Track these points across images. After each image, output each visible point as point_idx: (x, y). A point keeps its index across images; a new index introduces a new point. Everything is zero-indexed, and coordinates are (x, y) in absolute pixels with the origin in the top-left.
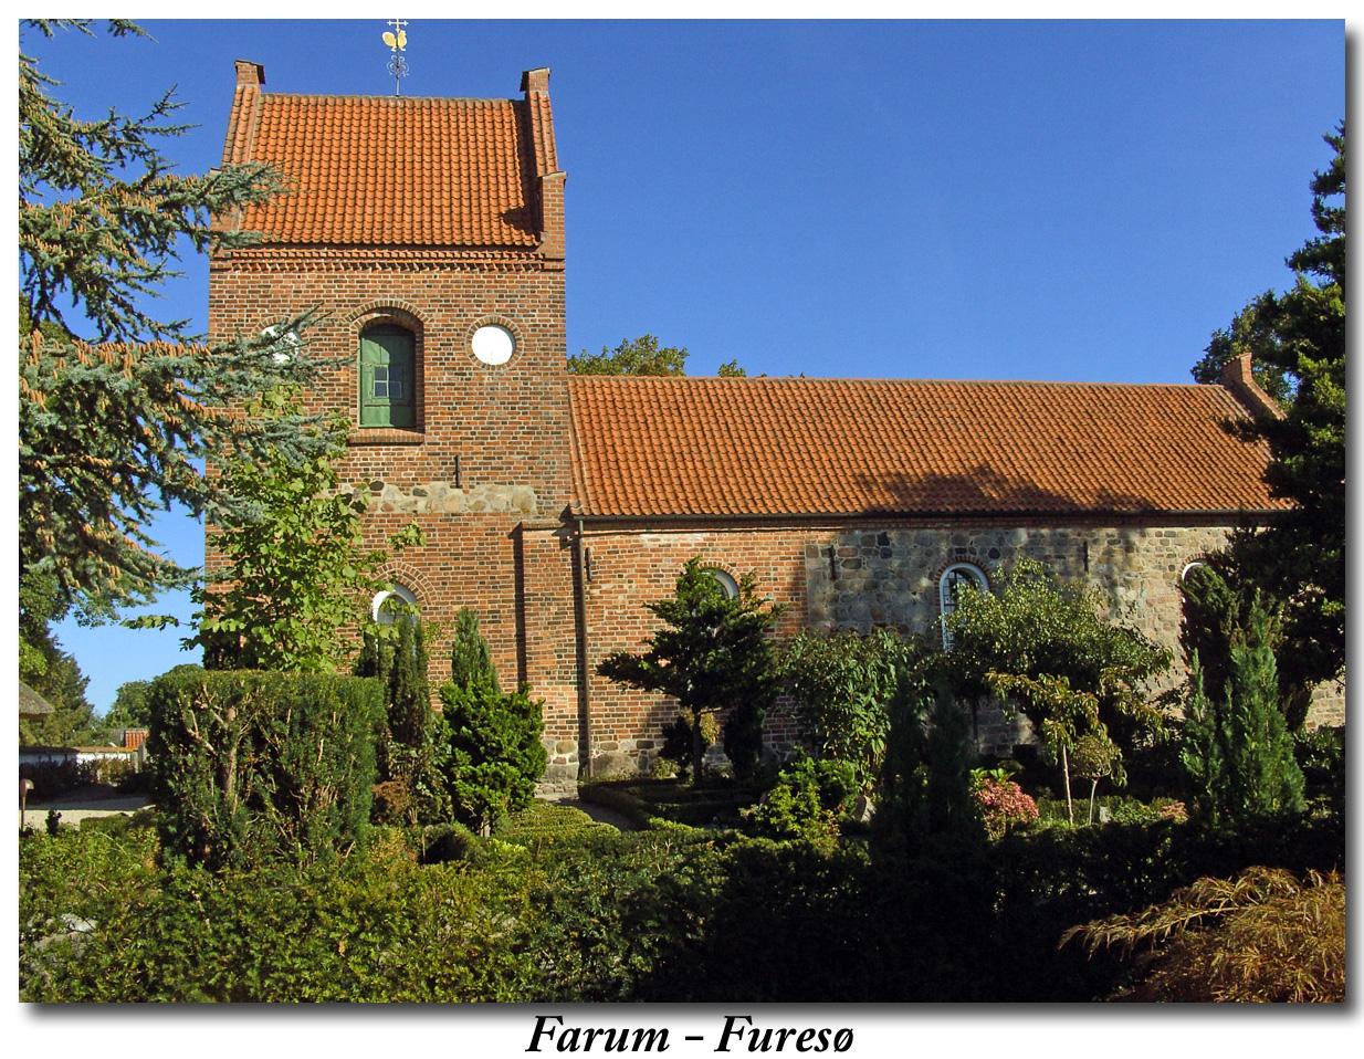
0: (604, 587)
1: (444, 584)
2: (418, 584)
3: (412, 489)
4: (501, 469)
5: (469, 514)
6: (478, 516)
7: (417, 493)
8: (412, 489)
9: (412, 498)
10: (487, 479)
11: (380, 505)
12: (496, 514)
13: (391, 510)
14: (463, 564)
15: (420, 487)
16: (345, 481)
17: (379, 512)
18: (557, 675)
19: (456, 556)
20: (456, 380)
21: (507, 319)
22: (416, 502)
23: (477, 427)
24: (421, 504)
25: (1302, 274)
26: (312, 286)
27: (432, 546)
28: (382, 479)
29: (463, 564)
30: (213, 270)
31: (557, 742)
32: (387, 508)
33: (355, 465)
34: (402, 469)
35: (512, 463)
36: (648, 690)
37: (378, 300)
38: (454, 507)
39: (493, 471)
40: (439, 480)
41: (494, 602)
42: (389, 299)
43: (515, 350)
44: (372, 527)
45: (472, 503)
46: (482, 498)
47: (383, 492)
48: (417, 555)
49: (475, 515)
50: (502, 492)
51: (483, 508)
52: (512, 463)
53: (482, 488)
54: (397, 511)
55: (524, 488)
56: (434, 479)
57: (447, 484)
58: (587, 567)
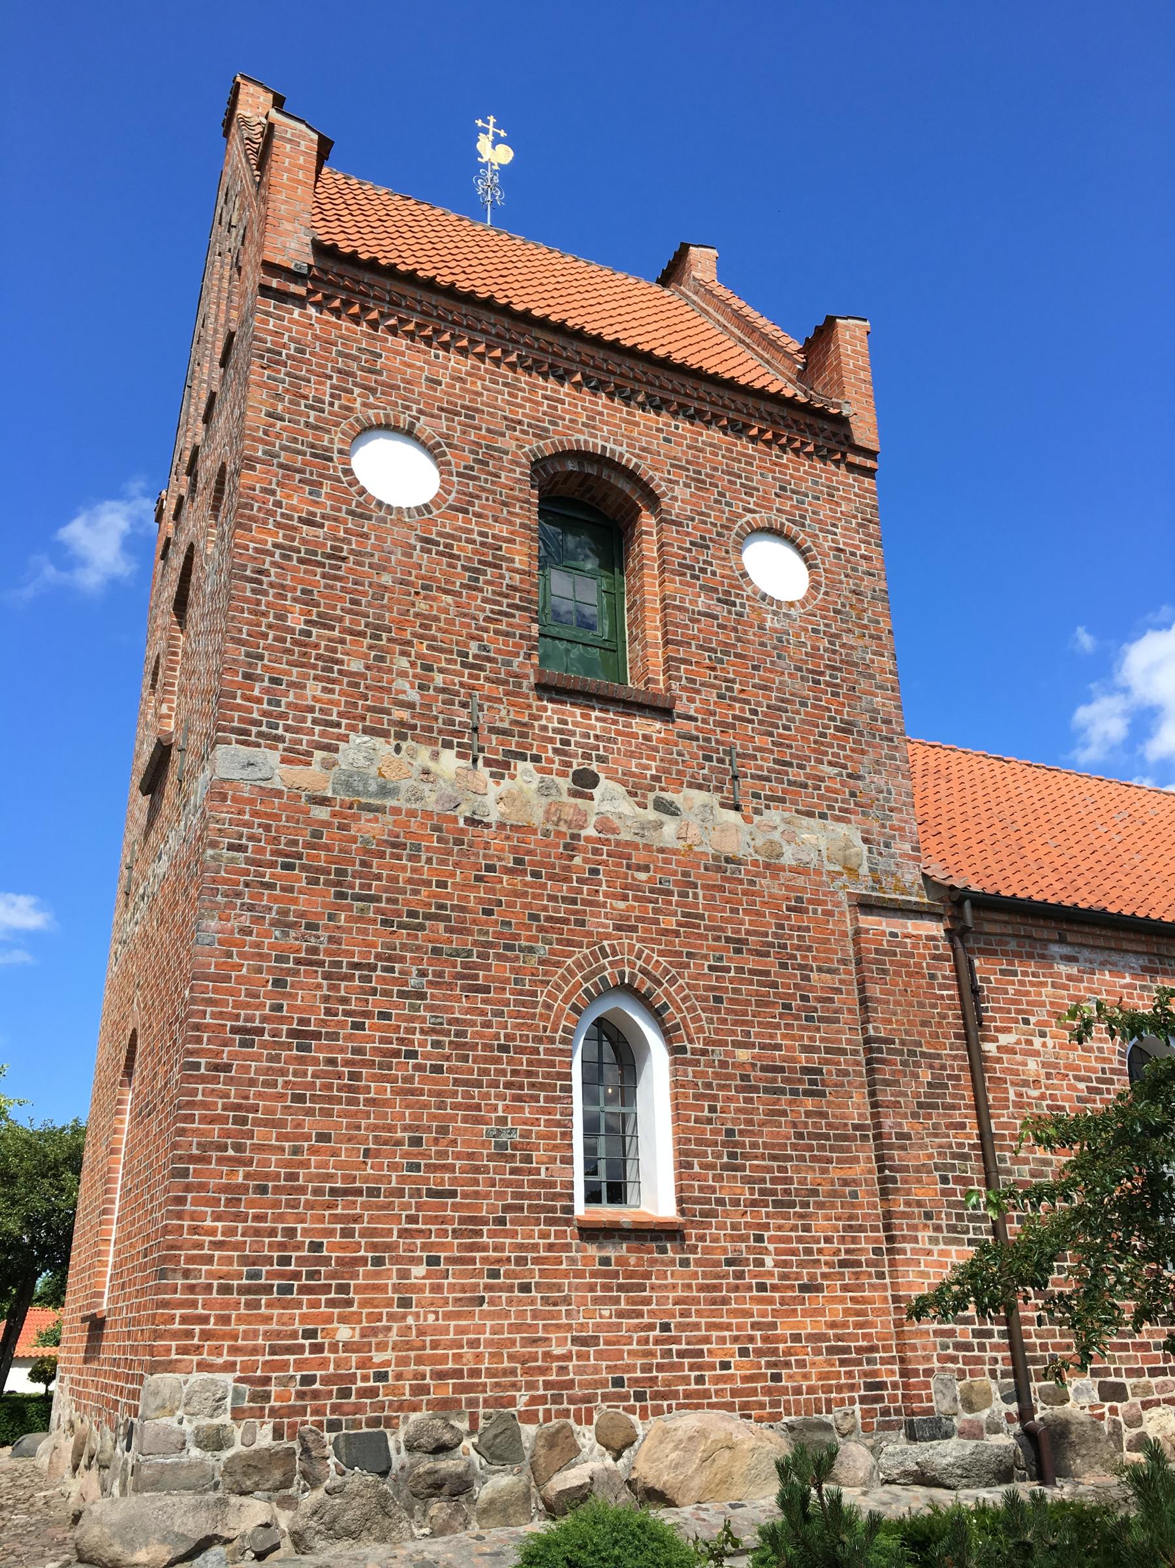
0: (1005, 1039)
1: (718, 1000)
2: (667, 994)
3: (651, 796)
4: (805, 786)
5: (755, 863)
6: (773, 868)
7: (662, 806)
8: (651, 796)
9: (651, 814)
10: (782, 800)
11: (593, 820)
12: (801, 869)
13: (614, 831)
14: (751, 962)
15: (668, 796)
16: (523, 757)
17: (590, 831)
18: (944, 1223)
19: (738, 945)
20: (721, 611)
21: (795, 528)
22: (660, 825)
23: (762, 702)
24: (670, 827)
25: (277, 1510)
26: (461, 380)
27: (691, 918)
28: (594, 766)
29: (751, 962)
30: (265, 290)
31: (959, 1386)
32: (605, 825)
33: (544, 728)
34: (632, 755)
35: (822, 779)
36: (453, 284)
37: (582, 438)
38: (730, 847)
39: (790, 790)
40: (700, 787)
41: (815, 1050)
42: (600, 442)
43: (815, 586)
44: (578, 860)
45: (759, 842)
46: (776, 836)
47: (596, 792)
48: (665, 932)
49: (767, 866)
50: (809, 829)
51: (780, 855)
52: (822, 779)
53: (774, 816)
54: (625, 836)
55: (841, 829)
56: (690, 785)
57: (714, 799)
58: (738, 316)
